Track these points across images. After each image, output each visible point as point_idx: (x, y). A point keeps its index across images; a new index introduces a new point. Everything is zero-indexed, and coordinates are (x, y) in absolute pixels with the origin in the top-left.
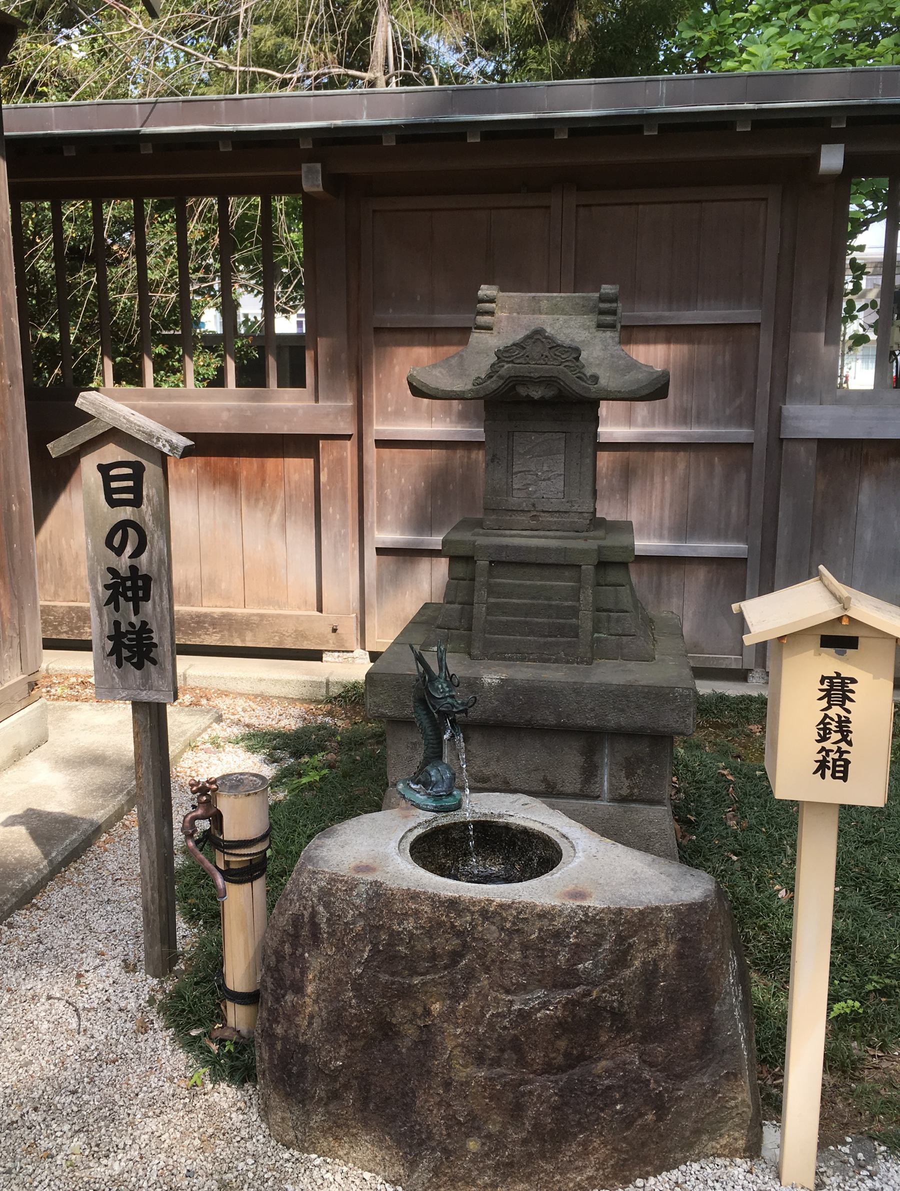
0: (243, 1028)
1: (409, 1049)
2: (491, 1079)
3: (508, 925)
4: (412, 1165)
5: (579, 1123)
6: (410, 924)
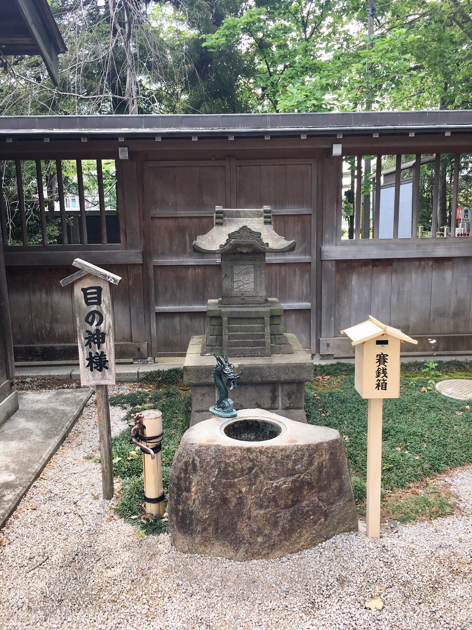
0: (154, 513)
1: (233, 507)
2: (266, 513)
3: (270, 455)
4: (237, 551)
5: (298, 526)
6: (233, 459)
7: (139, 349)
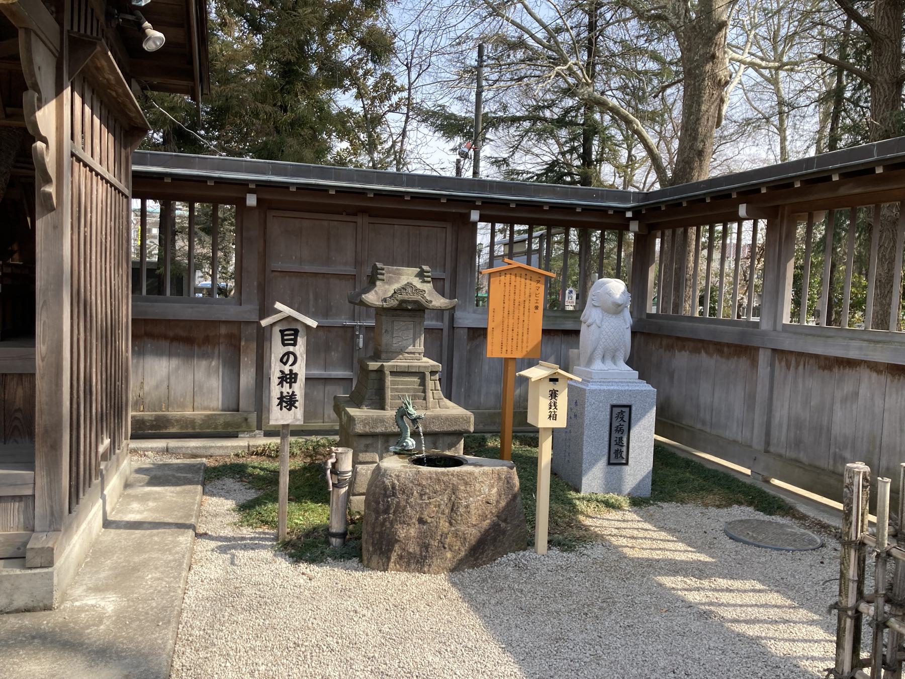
7: (246, 419)
